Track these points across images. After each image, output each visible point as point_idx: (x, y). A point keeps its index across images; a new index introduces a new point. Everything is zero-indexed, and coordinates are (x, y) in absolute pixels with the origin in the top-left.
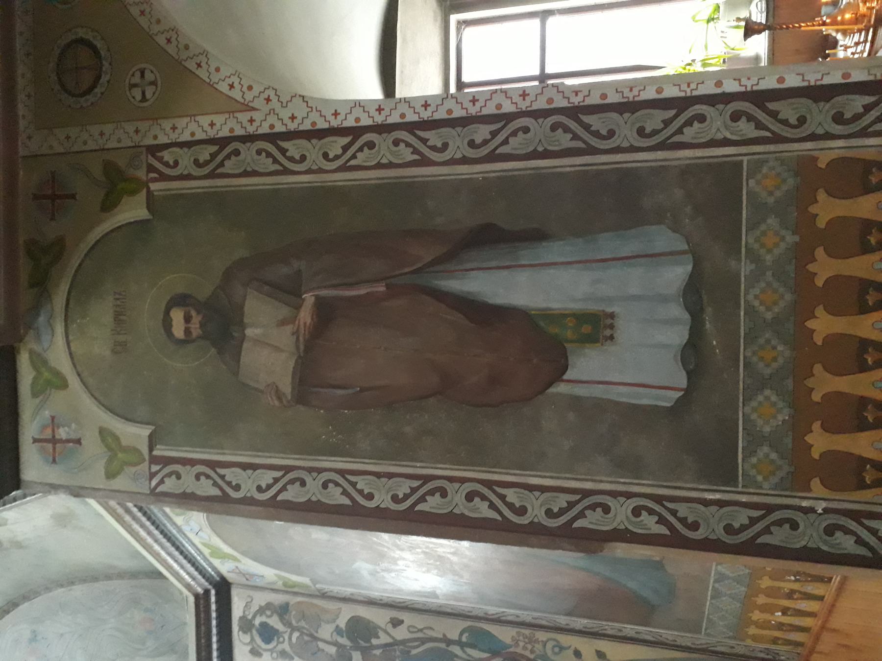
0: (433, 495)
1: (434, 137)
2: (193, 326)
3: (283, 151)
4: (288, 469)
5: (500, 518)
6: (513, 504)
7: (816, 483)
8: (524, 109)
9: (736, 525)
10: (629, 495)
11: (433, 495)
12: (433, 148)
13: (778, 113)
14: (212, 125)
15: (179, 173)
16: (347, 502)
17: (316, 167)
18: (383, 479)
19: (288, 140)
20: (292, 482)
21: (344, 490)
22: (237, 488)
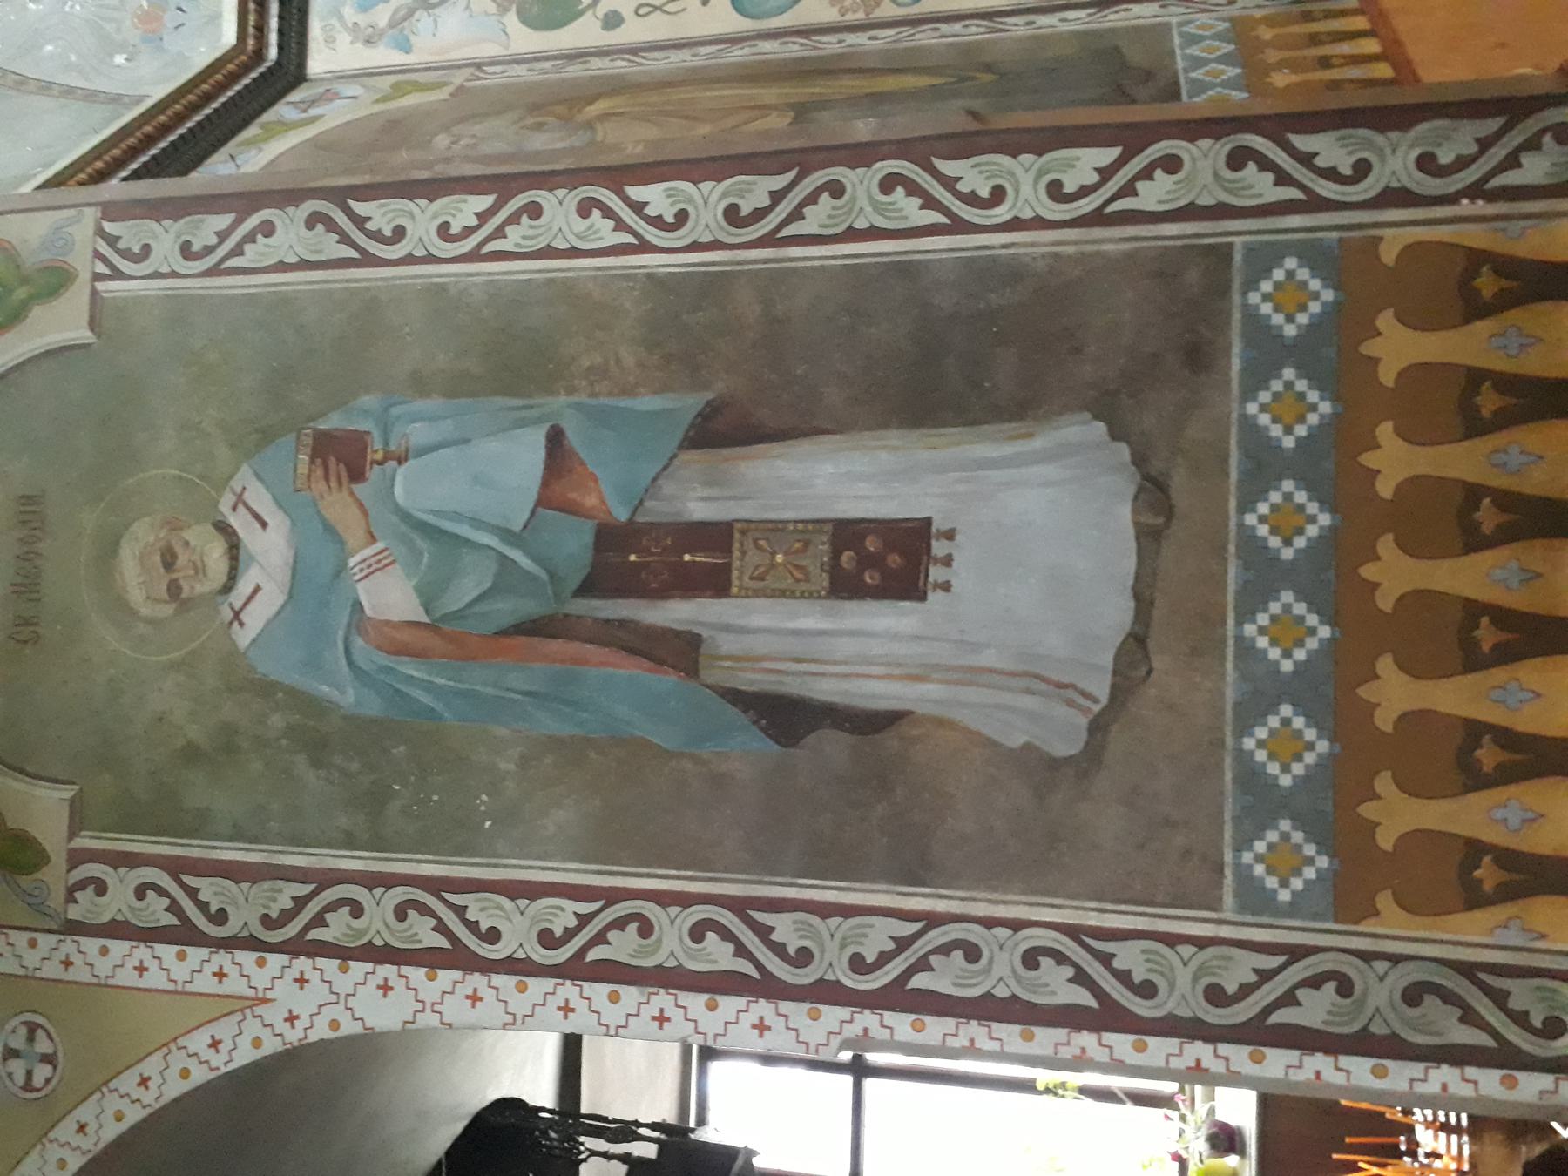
1: (717, 955)
2: (180, 575)
3: (174, 908)
6: (909, 194)
7: (1385, 901)
8: (568, 982)
10: (686, 900)
14: (141, 969)
17: (1180, 948)
18: (1210, 201)
19: (1067, 1008)
22: (1147, 990)
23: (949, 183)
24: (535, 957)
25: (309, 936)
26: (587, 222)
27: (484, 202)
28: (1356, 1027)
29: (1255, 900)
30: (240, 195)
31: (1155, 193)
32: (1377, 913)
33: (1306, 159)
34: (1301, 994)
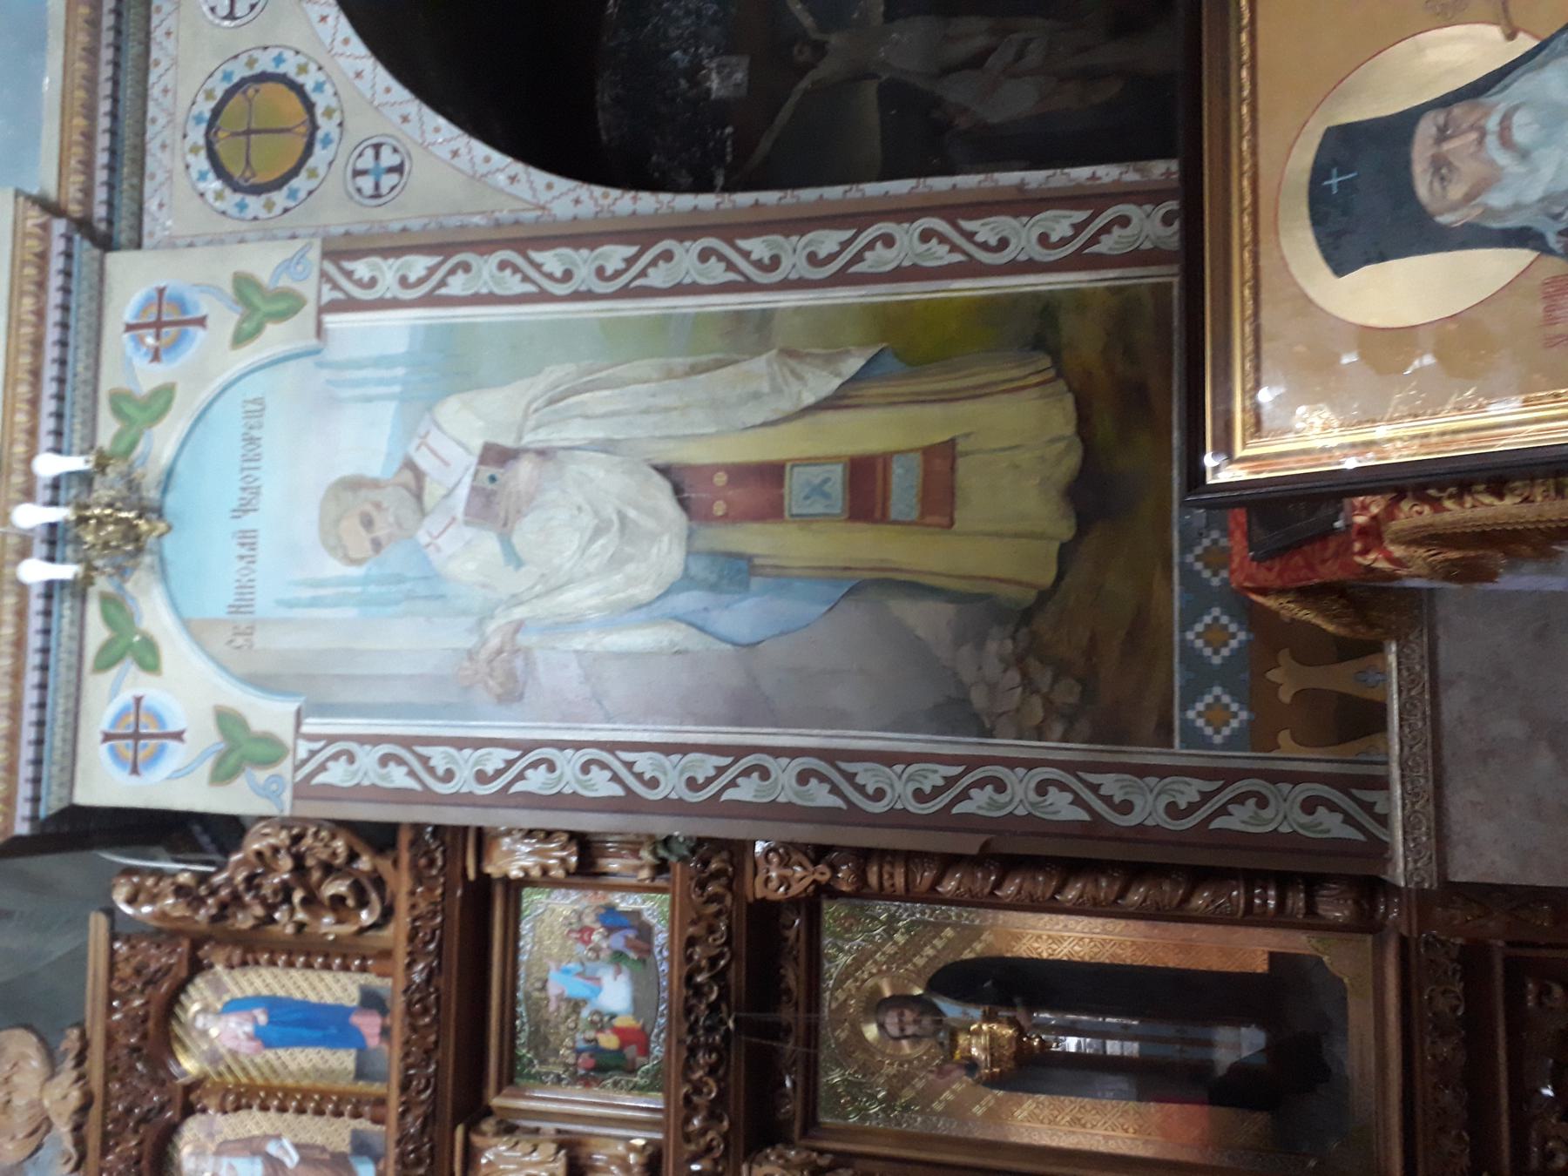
0: (1243, 804)
4: (739, 752)
5: (1361, 837)
7: (1284, 737)
9: (927, 789)
10: (1030, 764)
11: (1190, 803)
12: (984, 246)
13: (974, 234)
15: (782, 277)
16: (840, 803)
20: (746, 773)
21: (1076, 795)
23: (970, 236)
24: (911, 809)
25: (1213, 825)
26: (926, 246)
27: (1080, 216)
28: (555, 791)
29: (1193, 738)
30: (1155, 192)
31: (881, 259)
32: (1279, 747)
33: (970, 236)
34: (739, 780)
